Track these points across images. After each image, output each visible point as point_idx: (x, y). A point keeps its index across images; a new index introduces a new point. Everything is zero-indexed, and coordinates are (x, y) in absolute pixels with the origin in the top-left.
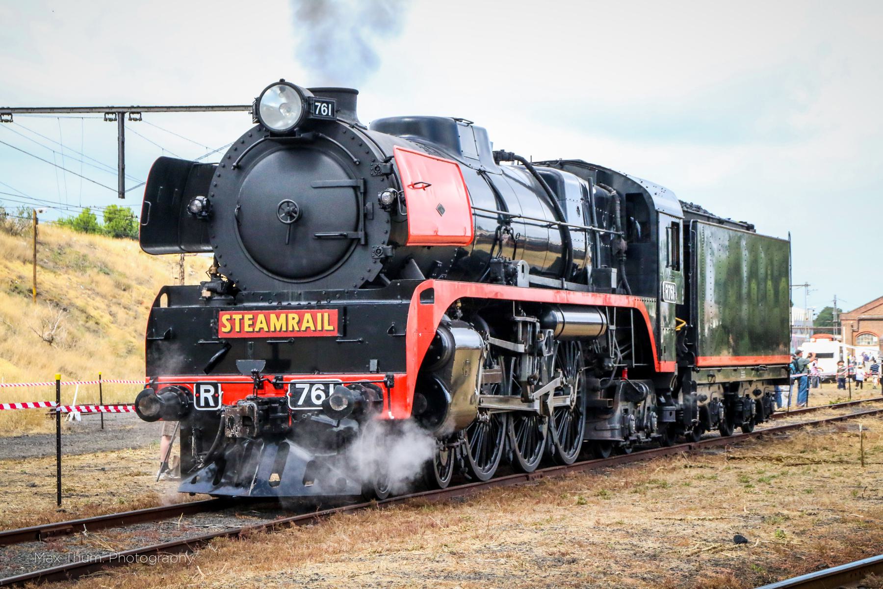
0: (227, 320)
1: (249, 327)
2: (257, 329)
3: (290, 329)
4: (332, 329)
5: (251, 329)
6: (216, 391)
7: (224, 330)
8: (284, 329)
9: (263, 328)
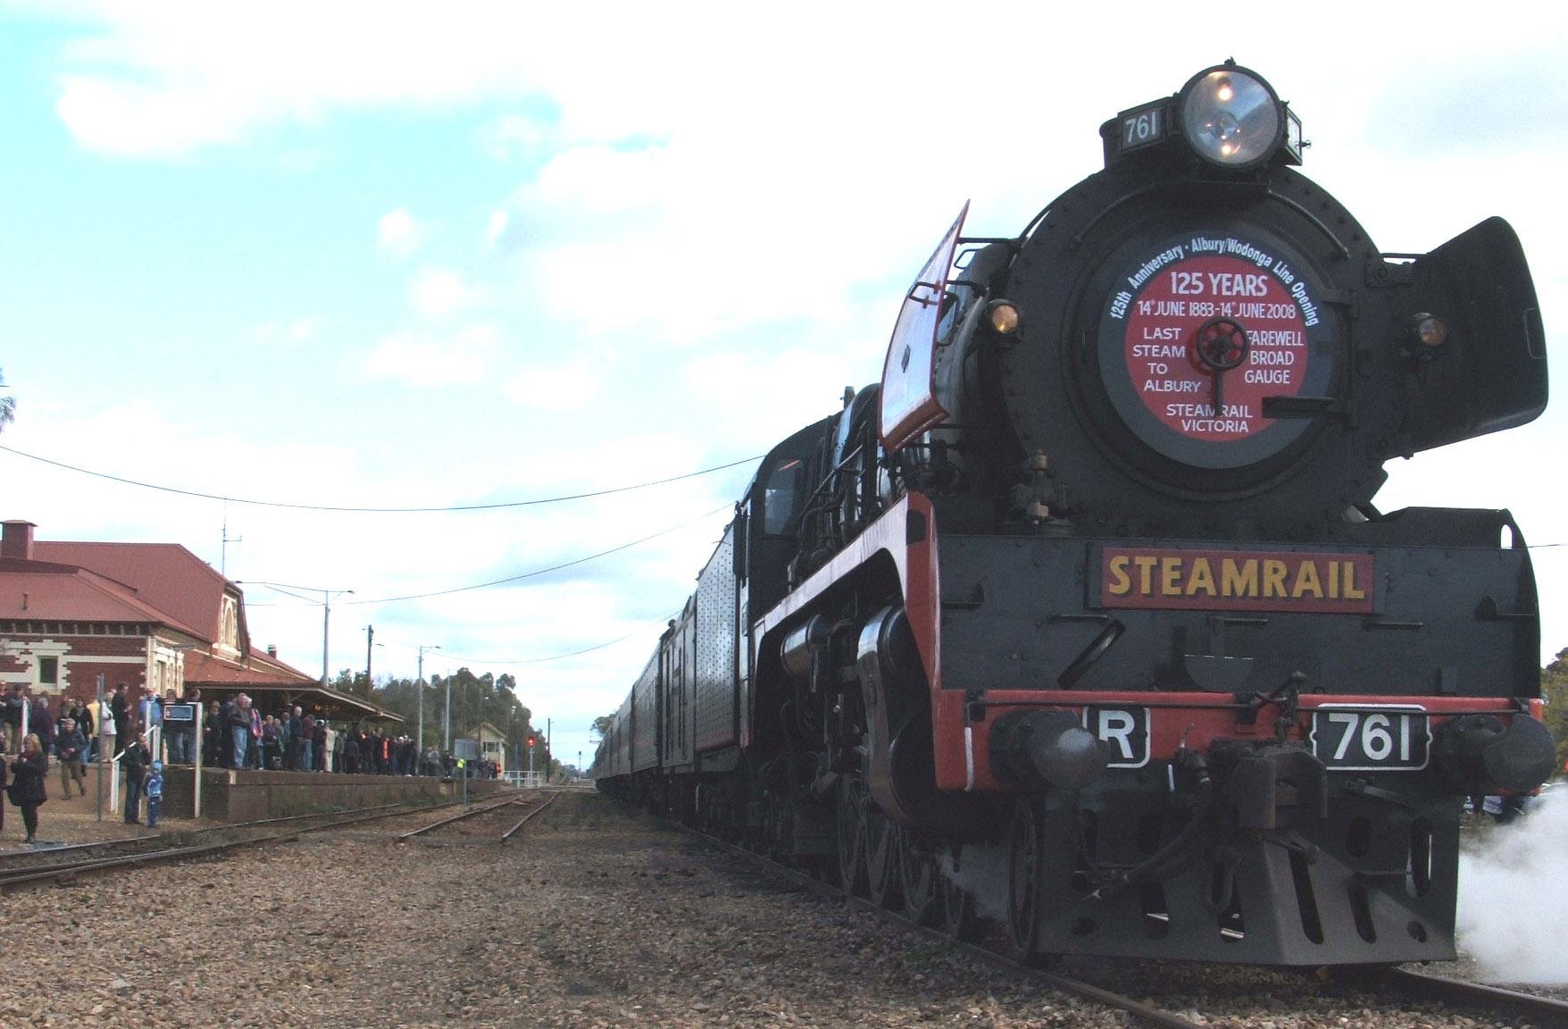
0: (1122, 567)
1: (1173, 585)
2: (1191, 590)
3: (1268, 592)
4: (1363, 597)
5: (1177, 591)
6: (1140, 723)
7: (1114, 589)
8: (1253, 592)
9: (1205, 589)
